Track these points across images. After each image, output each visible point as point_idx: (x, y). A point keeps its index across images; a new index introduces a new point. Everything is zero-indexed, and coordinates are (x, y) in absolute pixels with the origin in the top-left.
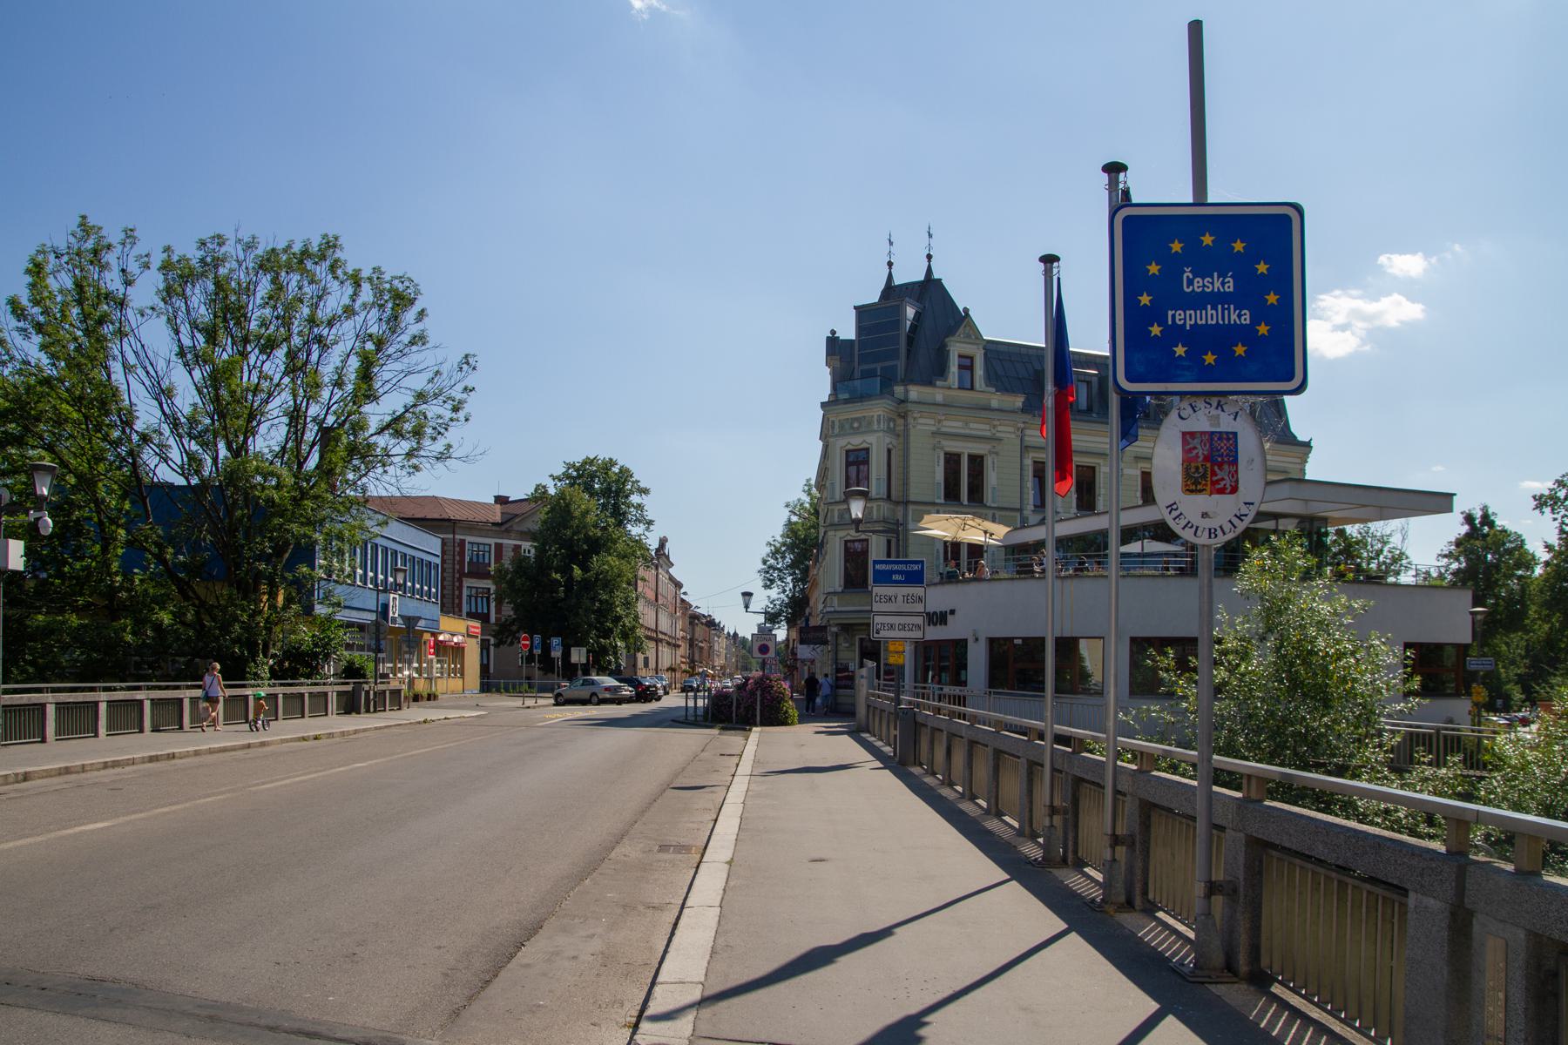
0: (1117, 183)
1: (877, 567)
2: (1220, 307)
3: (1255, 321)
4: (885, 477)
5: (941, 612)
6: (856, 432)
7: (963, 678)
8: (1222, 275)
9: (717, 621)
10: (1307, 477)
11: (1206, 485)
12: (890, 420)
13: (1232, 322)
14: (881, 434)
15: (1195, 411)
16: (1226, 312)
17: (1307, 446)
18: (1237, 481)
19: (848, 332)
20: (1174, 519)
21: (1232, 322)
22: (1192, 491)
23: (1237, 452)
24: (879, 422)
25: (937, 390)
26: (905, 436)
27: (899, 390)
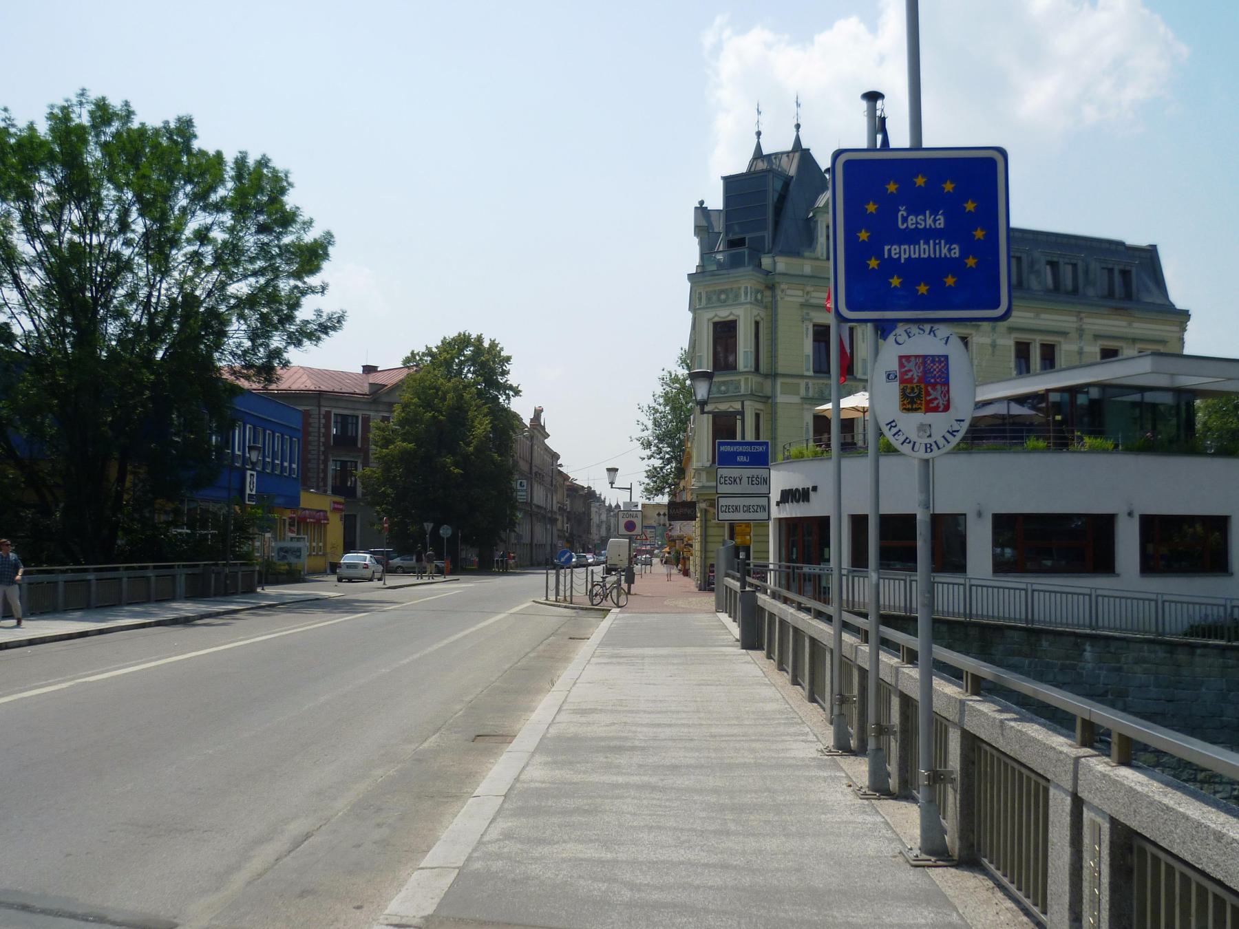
0: (875, 110)
1: (722, 448)
2: (931, 242)
3: (964, 254)
4: (753, 350)
5: (803, 489)
6: (723, 304)
7: (827, 557)
8: (934, 213)
9: (598, 492)
10: (1187, 351)
11: (921, 404)
12: (757, 292)
13: (943, 256)
14: (748, 306)
15: (910, 337)
16: (937, 247)
17: (1185, 315)
18: (948, 401)
19: (716, 201)
20: (894, 435)
21: (943, 256)
22: (908, 410)
23: (948, 374)
24: (746, 294)
25: (807, 262)
26: (772, 308)
27: (766, 261)
